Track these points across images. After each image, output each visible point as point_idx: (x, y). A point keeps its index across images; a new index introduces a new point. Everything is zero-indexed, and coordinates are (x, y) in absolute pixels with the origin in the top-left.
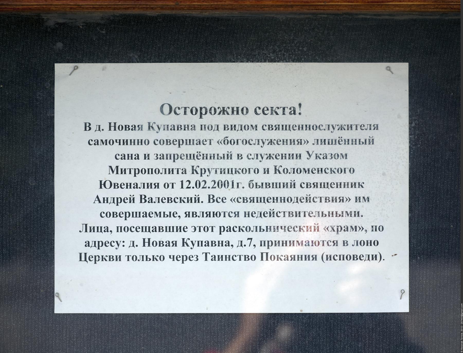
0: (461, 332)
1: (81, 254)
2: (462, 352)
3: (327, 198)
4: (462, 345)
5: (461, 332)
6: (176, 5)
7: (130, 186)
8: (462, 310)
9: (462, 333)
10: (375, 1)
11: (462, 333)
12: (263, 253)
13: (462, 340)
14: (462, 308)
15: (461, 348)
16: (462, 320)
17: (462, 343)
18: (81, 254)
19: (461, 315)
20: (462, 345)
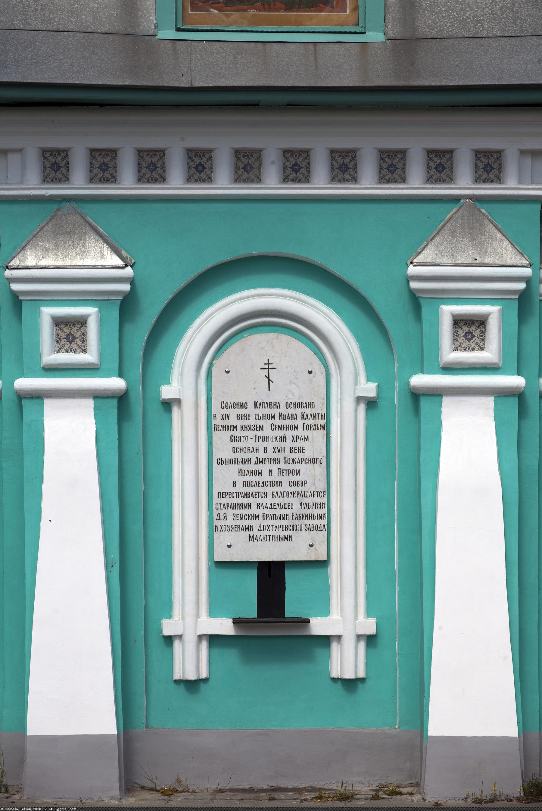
0: (32, 809)
1: (286, 441)
2: (2, 809)
3: (319, 470)
4: (12, 809)
5: (32, 809)
6: (382, 787)
7: (188, 88)
8: (66, 809)
9: (30, 809)
10: (311, 787)
11: (30, 809)
12: (290, 575)
13: (20, 809)
14: (69, 809)
15: (8, 808)
16: (51, 809)
17: (16, 809)
18: (286, 441)
19: (58, 808)
20: (12, 809)
